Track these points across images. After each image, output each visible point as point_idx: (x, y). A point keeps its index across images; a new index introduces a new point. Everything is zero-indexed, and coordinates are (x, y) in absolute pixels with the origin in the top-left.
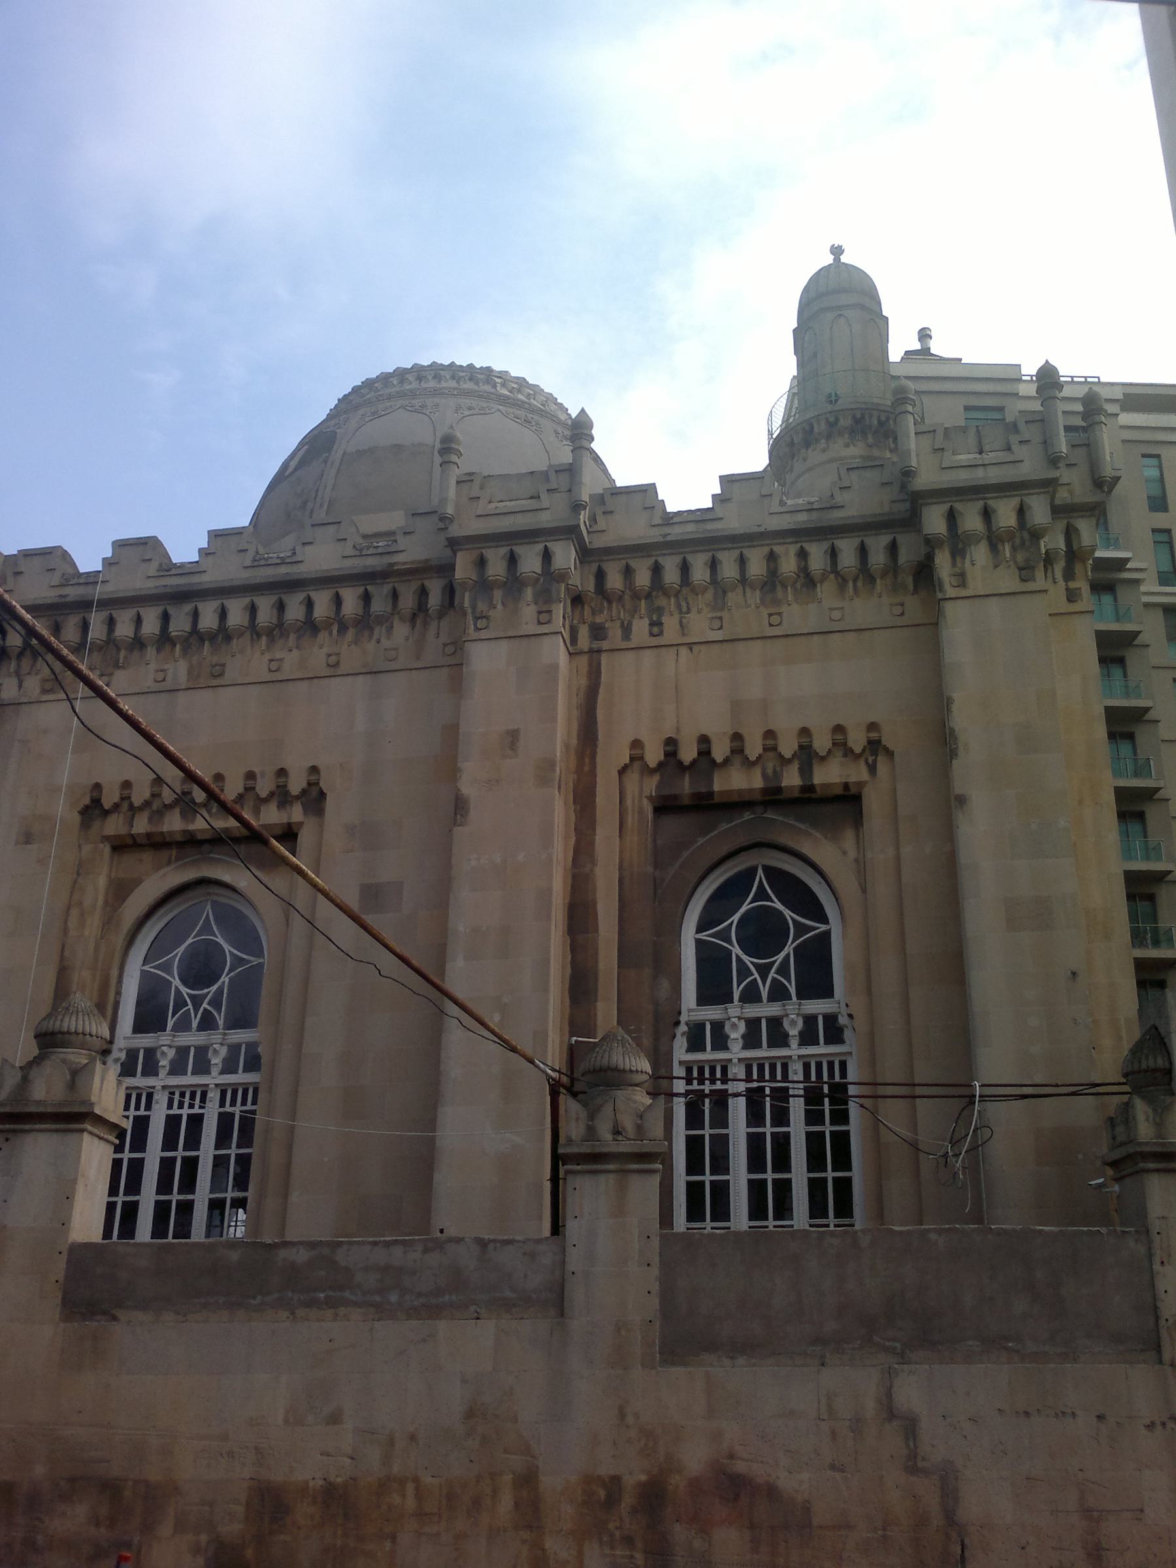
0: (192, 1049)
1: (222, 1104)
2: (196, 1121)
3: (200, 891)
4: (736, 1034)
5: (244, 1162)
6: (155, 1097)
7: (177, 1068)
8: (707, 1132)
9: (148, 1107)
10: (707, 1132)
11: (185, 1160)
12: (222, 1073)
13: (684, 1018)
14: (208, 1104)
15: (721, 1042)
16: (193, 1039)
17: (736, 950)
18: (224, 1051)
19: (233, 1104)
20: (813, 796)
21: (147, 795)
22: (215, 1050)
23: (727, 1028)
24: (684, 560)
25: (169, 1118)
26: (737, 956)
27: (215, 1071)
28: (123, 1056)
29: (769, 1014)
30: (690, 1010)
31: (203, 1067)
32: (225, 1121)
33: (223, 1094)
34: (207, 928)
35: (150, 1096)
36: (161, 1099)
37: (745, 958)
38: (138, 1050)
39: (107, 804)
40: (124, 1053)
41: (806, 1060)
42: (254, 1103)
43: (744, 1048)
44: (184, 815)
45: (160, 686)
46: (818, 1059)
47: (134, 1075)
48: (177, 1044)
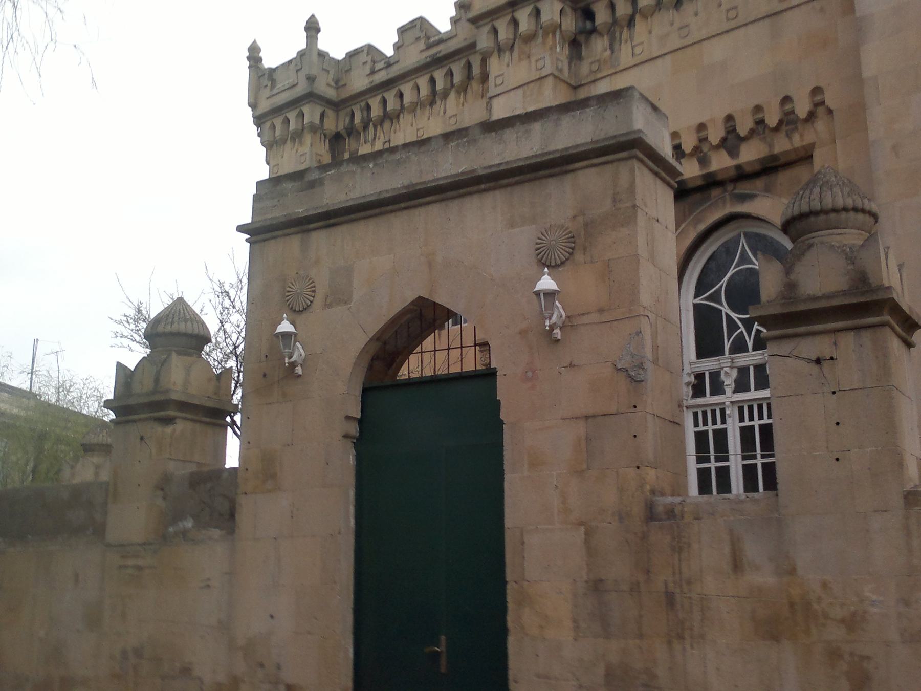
0: (752, 369)
1: (696, 424)
2: (721, 436)
3: (732, 225)
4: (729, 381)
5: (769, 470)
6: (728, 412)
7: (741, 385)
8: (759, 461)
9: (724, 421)
10: (759, 461)
11: (718, 469)
12: (735, 392)
13: (687, 369)
14: (729, 420)
15: (717, 389)
16: (751, 358)
17: (725, 309)
18: (734, 374)
19: (705, 424)
20: (778, 163)
21: (721, 133)
22: (726, 373)
23: (723, 376)
24: (416, 83)
25: (698, 435)
26: (726, 314)
27: (729, 391)
28: (692, 379)
29: (754, 362)
30: (691, 364)
31: (717, 389)
32: (747, 434)
33: (741, 410)
34: (744, 259)
35: (723, 412)
36: (732, 413)
37: (734, 316)
38: (747, 368)
39: (743, 131)
40: (693, 376)
41: (741, 405)
42: (769, 417)
43: (735, 392)
44: (789, 136)
45: (733, 24)
46: (750, 404)
47: (704, 395)
48: (739, 365)
